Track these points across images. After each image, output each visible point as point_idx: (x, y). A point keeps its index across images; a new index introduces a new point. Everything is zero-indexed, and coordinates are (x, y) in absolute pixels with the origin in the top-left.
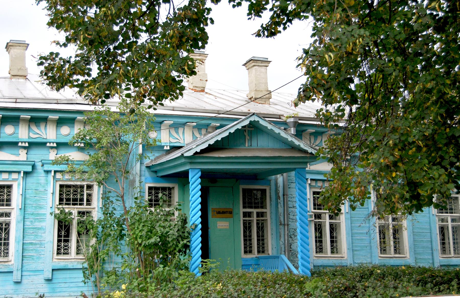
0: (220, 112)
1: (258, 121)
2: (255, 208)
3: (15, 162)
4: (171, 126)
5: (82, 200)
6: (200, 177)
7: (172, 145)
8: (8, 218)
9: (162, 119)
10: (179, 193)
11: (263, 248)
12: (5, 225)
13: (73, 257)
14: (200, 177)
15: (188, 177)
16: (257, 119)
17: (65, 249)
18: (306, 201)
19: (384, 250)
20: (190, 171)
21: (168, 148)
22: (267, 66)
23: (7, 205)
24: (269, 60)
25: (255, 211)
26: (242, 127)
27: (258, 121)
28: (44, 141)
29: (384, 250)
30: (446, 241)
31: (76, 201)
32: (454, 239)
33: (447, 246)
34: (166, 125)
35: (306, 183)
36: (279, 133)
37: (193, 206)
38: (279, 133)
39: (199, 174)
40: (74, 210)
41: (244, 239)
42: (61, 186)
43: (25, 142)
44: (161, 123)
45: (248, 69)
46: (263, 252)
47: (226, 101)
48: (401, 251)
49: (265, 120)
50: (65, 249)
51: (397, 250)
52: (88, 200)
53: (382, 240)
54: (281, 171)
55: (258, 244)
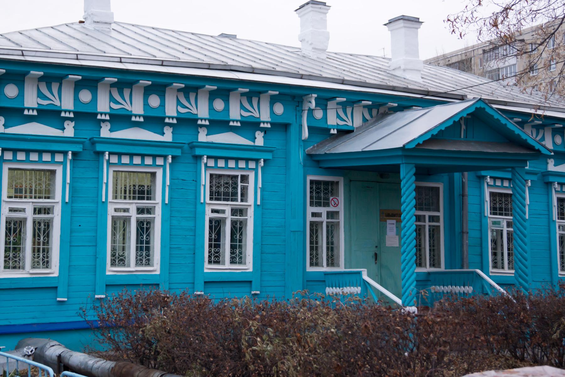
0: (396, 89)
1: (484, 109)
2: (428, 210)
3: (147, 143)
4: (41, 79)
5: (235, 194)
6: (415, 174)
7: (339, 128)
8: (149, 216)
9: (64, 72)
10: (344, 189)
11: (241, 258)
12: (147, 225)
13: (227, 267)
14: (415, 174)
15: (399, 172)
16: (483, 106)
17: (217, 257)
18: (525, 207)
19: (122, 260)
20: (401, 166)
21: (335, 132)
22: (417, 28)
23: (148, 199)
24: (420, 20)
25: (427, 214)
26: (468, 115)
27: (484, 109)
28: (257, 120)
29: (122, 260)
30: (499, 252)
31: (231, 196)
32: (509, 249)
33: (499, 257)
34: (70, 81)
35: (525, 186)
36: (506, 125)
37: (407, 209)
38: (506, 125)
39: (414, 171)
40: (226, 207)
41: (310, 247)
42: (211, 175)
43: (105, 114)
44: (166, 86)
45: (391, 31)
46: (217, 262)
47: (177, 52)
48: (335, 261)
49: (492, 108)
50: (217, 257)
51: (332, 261)
52: (242, 195)
53: (36, 246)
54: (462, 169)
55: (311, 254)
